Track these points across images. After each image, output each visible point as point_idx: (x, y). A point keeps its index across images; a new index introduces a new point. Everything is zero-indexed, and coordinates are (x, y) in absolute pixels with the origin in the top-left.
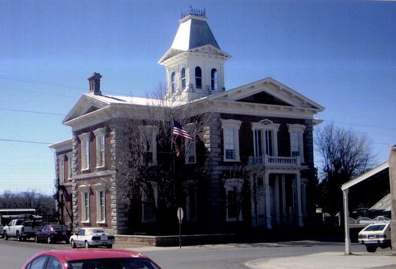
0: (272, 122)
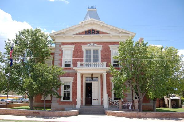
0: (96, 45)
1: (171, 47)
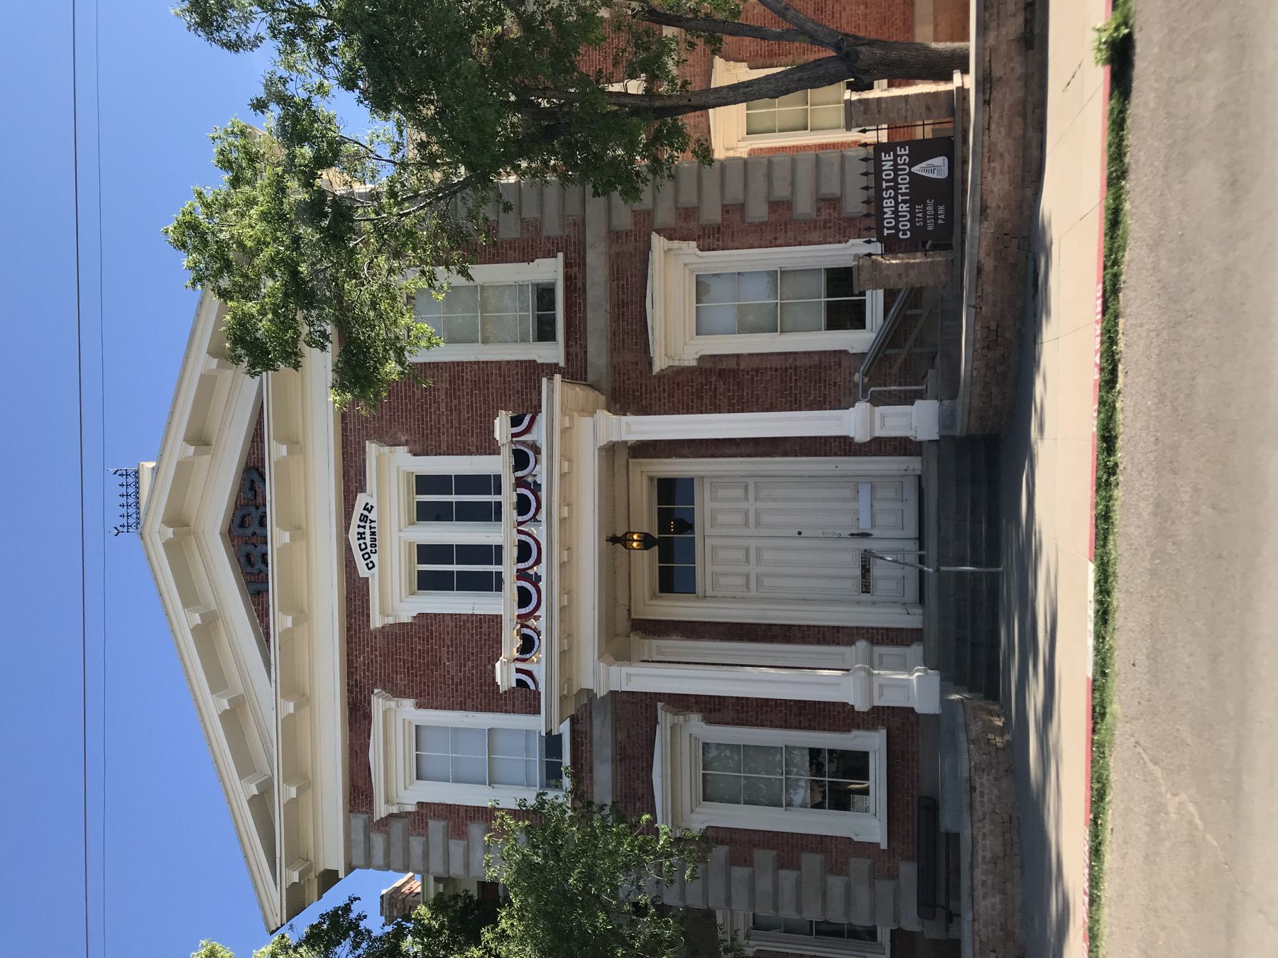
0: (361, 500)
1: (1103, 900)
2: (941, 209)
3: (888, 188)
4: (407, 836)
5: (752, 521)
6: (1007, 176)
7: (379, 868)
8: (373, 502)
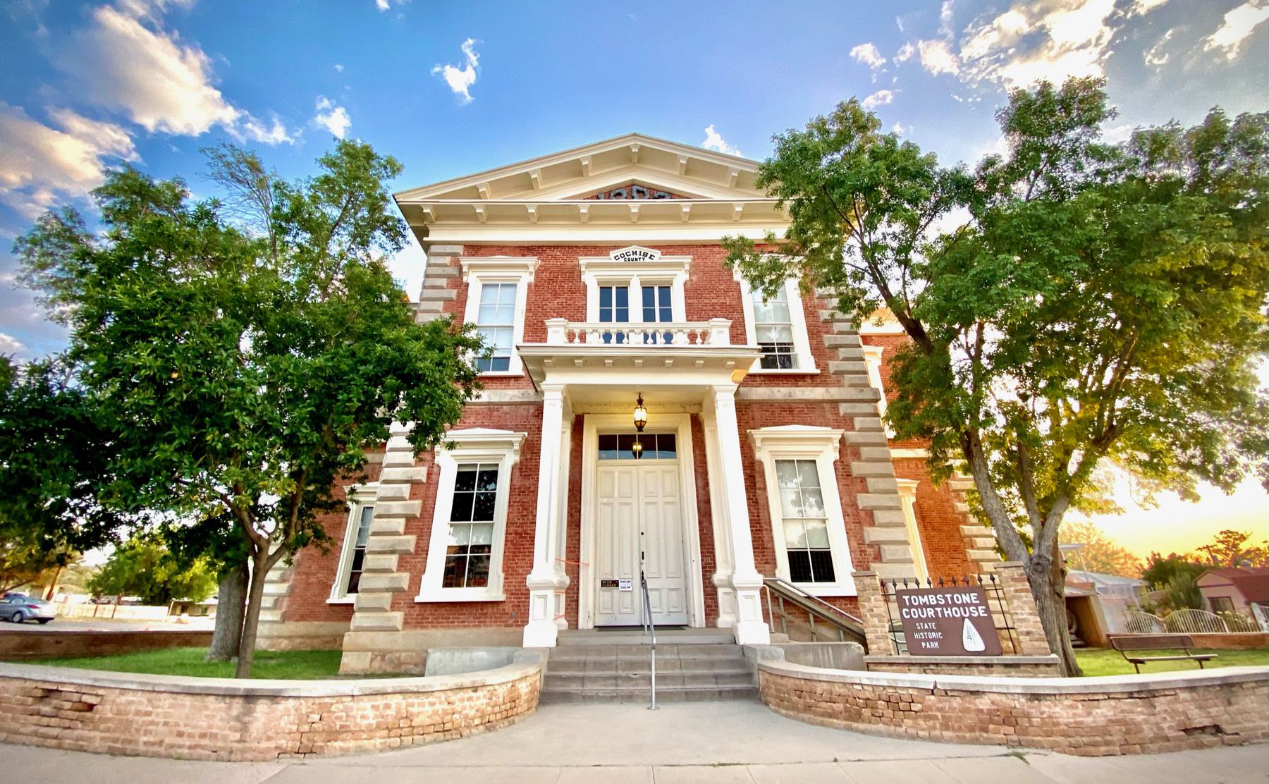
0: (657, 254)
2: (935, 645)
3: (946, 599)
4: (448, 277)
5: (654, 500)
6: (1072, 720)
7: (424, 282)
8: (655, 260)
